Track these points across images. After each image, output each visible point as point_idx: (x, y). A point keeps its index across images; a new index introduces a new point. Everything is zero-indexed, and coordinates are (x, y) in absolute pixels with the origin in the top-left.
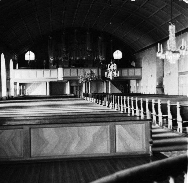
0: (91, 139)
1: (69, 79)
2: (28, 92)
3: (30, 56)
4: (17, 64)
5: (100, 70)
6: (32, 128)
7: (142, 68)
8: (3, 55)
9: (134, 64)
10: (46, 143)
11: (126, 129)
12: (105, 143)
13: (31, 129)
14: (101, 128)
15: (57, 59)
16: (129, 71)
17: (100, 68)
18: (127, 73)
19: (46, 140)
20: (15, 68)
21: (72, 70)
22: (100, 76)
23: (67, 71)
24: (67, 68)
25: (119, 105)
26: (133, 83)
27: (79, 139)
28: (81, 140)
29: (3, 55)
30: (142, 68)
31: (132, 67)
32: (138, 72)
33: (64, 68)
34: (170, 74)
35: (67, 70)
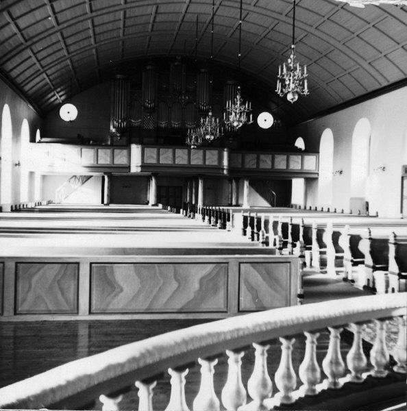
0: (196, 286)
1: (155, 170)
2: (60, 196)
3: (69, 113)
4: (38, 131)
5: (225, 154)
6: (243, 263)
7: (319, 152)
8: (6, 108)
9: (300, 143)
10: (117, 290)
11: (258, 271)
12: (20, 298)
13: (241, 265)
14: (61, 267)
15: (129, 123)
16: (276, 160)
17: (226, 150)
18: (285, 162)
19: (119, 286)
20: (33, 140)
21: (117, 151)
22: (225, 167)
23: (151, 153)
24: (153, 145)
25: (255, 230)
26: (298, 185)
27: (175, 285)
28: (179, 287)
29: (6, 108)
30: (320, 154)
31: (298, 151)
32: (310, 163)
33: (144, 145)
34: (341, 172)
35: (151, 149)
